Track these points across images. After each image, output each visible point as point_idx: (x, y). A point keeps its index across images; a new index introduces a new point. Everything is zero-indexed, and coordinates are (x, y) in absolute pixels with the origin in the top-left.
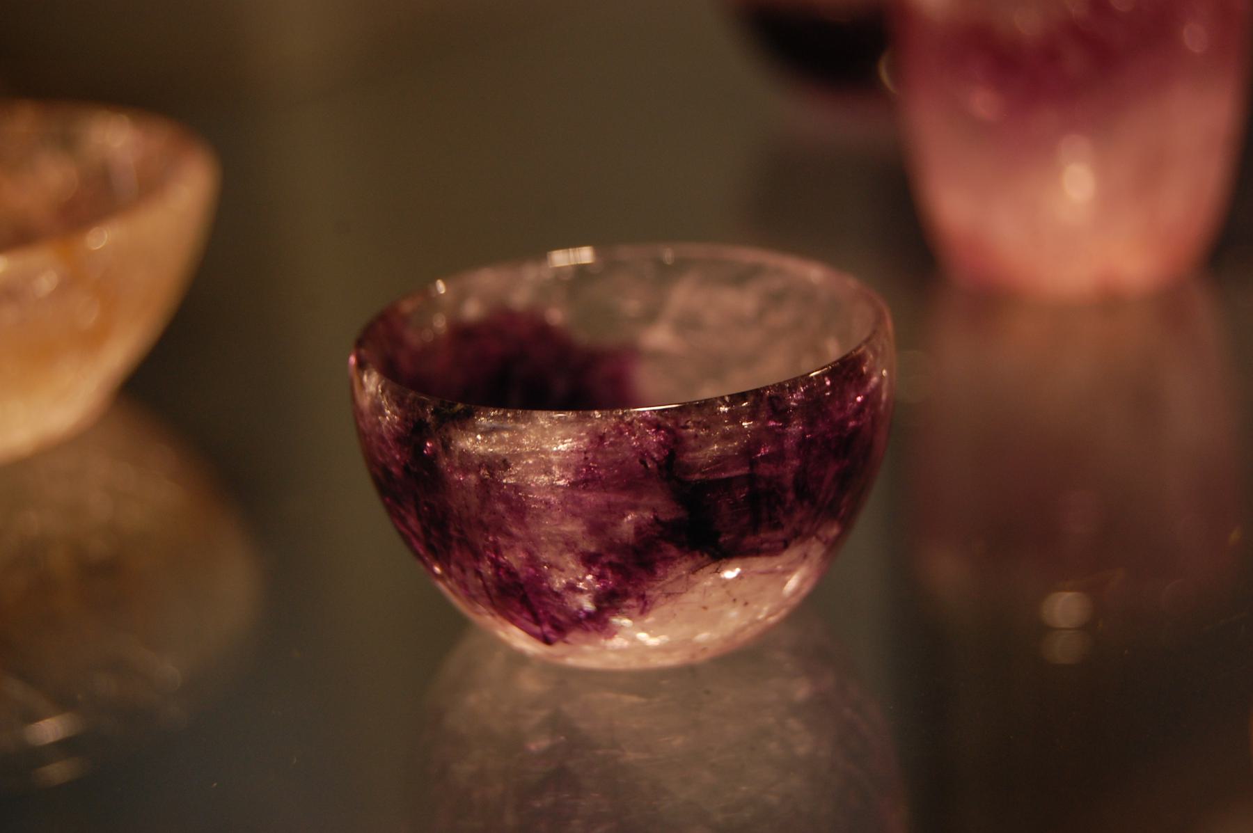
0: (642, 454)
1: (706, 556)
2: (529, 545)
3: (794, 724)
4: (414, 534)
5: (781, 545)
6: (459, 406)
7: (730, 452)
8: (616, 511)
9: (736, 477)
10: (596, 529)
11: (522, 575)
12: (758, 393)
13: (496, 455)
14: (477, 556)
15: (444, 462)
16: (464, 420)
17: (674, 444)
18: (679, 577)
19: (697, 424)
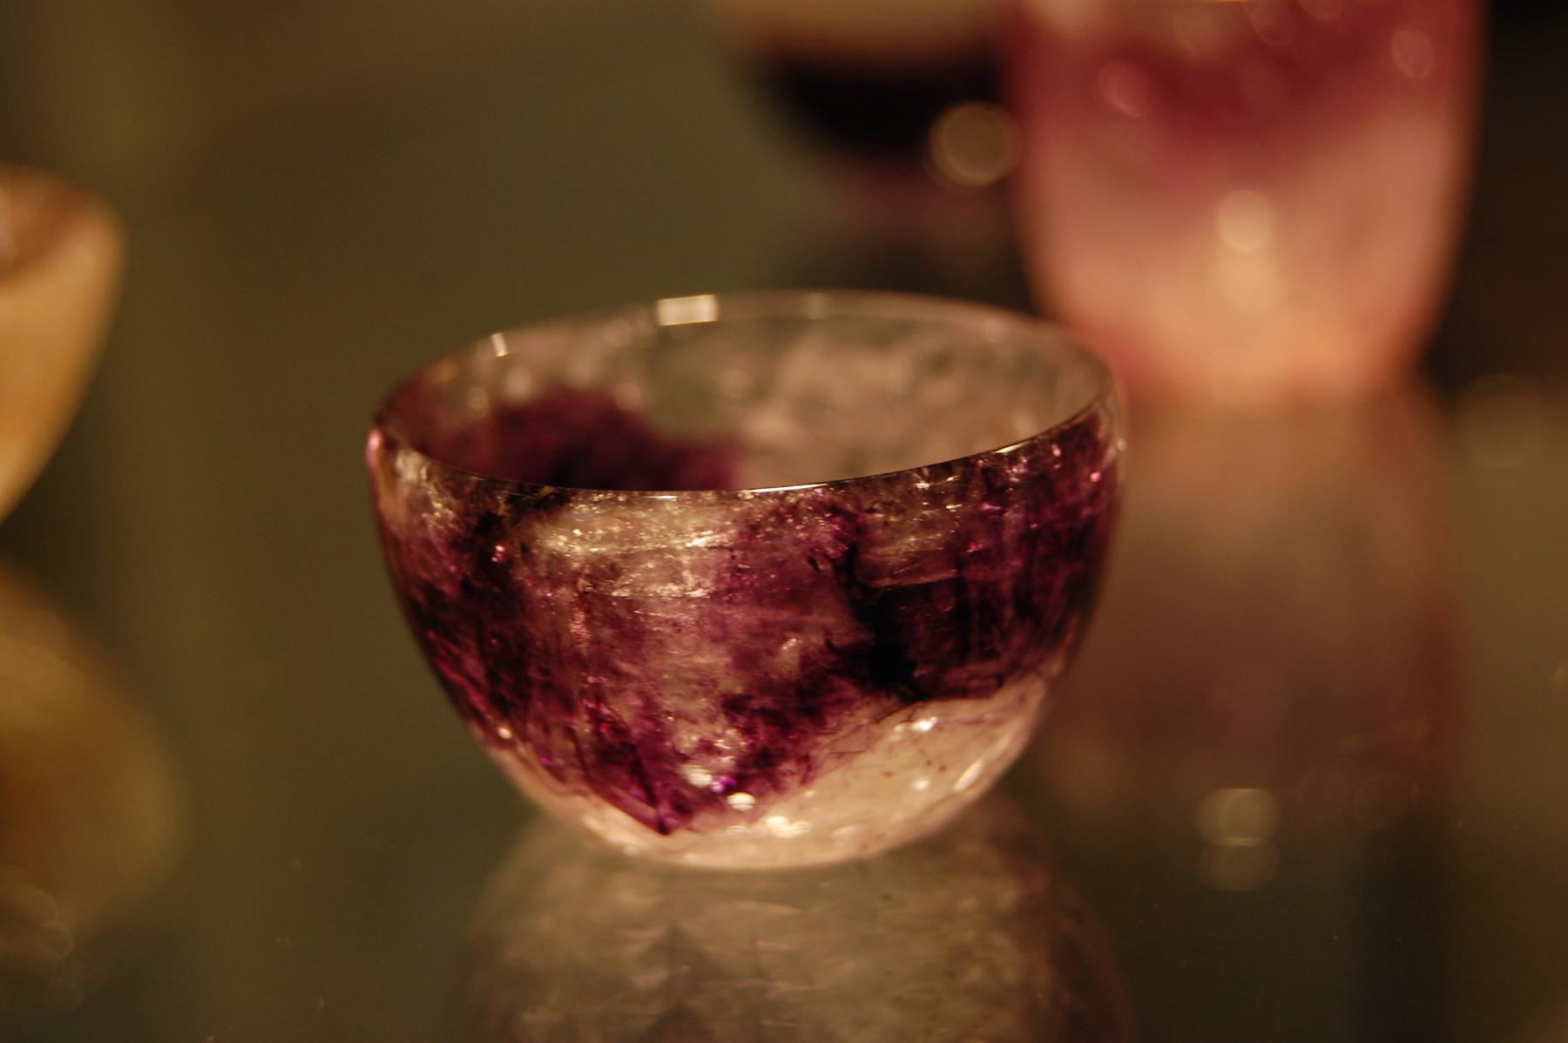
0: (812, 550)
1: (894, 699)
2: (648, 688)
3: (1002, 941)
4: (472, 680)
5: (993, 682)
6: (548, 490)
7: (933, 547)
8: (771, 634)
9: (940, 582)
10: (745, 660)
11: (635, 731)
12: (967, 463)
13: (602, 558)
14: (569, 707)
15: (522, 574)
16: (553, 509)
17: (856, 537)
18: (858, 728)
19: (888, 507)
